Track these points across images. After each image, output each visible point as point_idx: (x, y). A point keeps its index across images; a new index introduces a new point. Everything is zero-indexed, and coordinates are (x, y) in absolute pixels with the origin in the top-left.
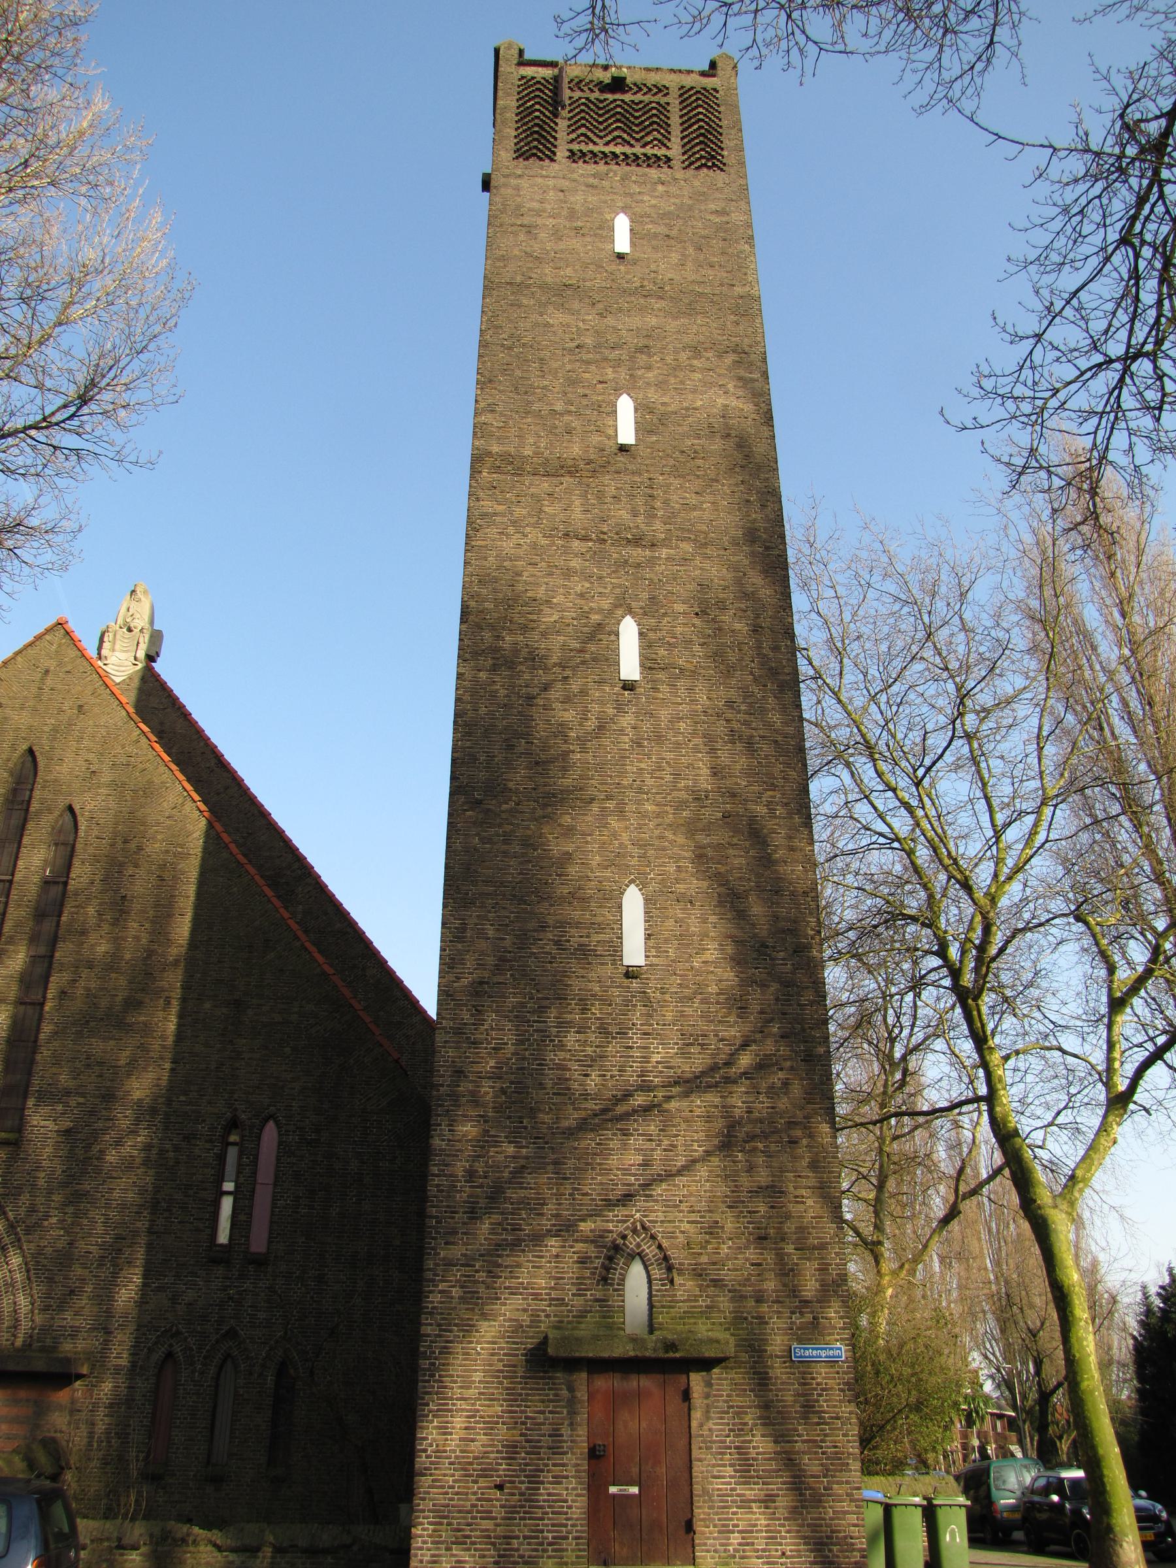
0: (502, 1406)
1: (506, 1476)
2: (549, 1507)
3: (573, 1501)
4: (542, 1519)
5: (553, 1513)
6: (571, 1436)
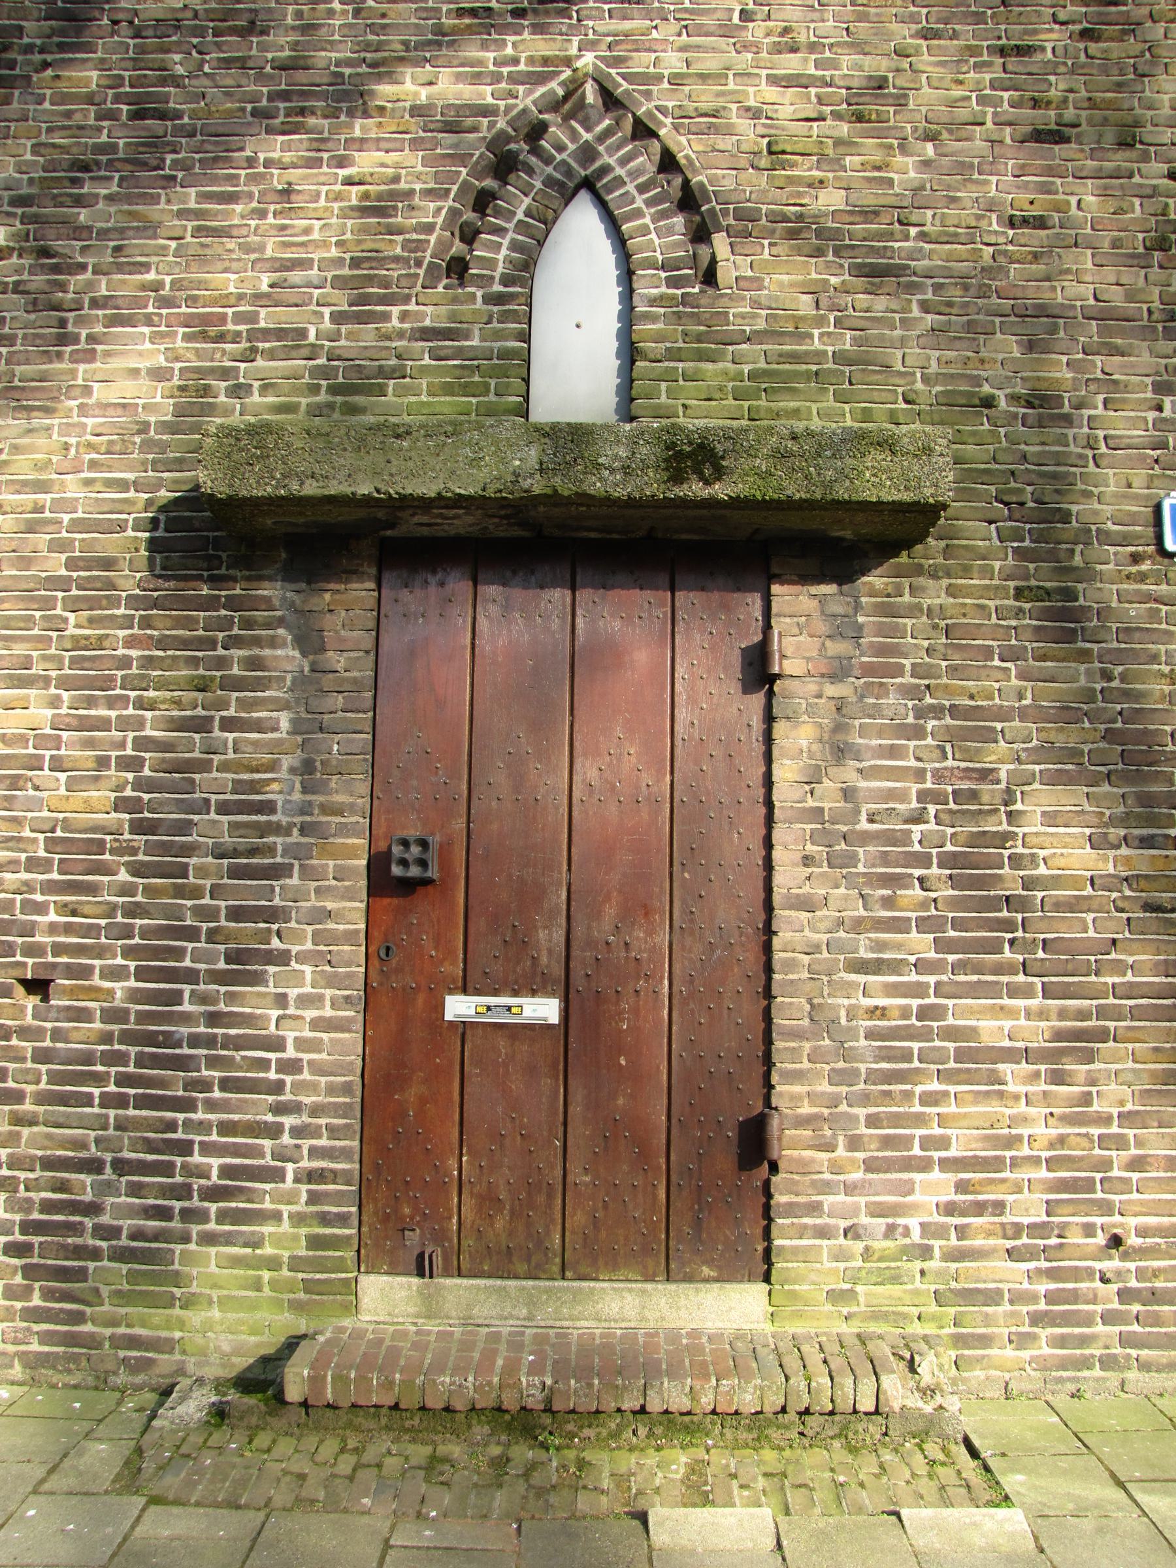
0: (55, 702)
1: (58, 949)
2: (213, 1062)
3: (300, 1044)
4: (187, 1105)
5: (225, 1084)
6: (305, 809)
